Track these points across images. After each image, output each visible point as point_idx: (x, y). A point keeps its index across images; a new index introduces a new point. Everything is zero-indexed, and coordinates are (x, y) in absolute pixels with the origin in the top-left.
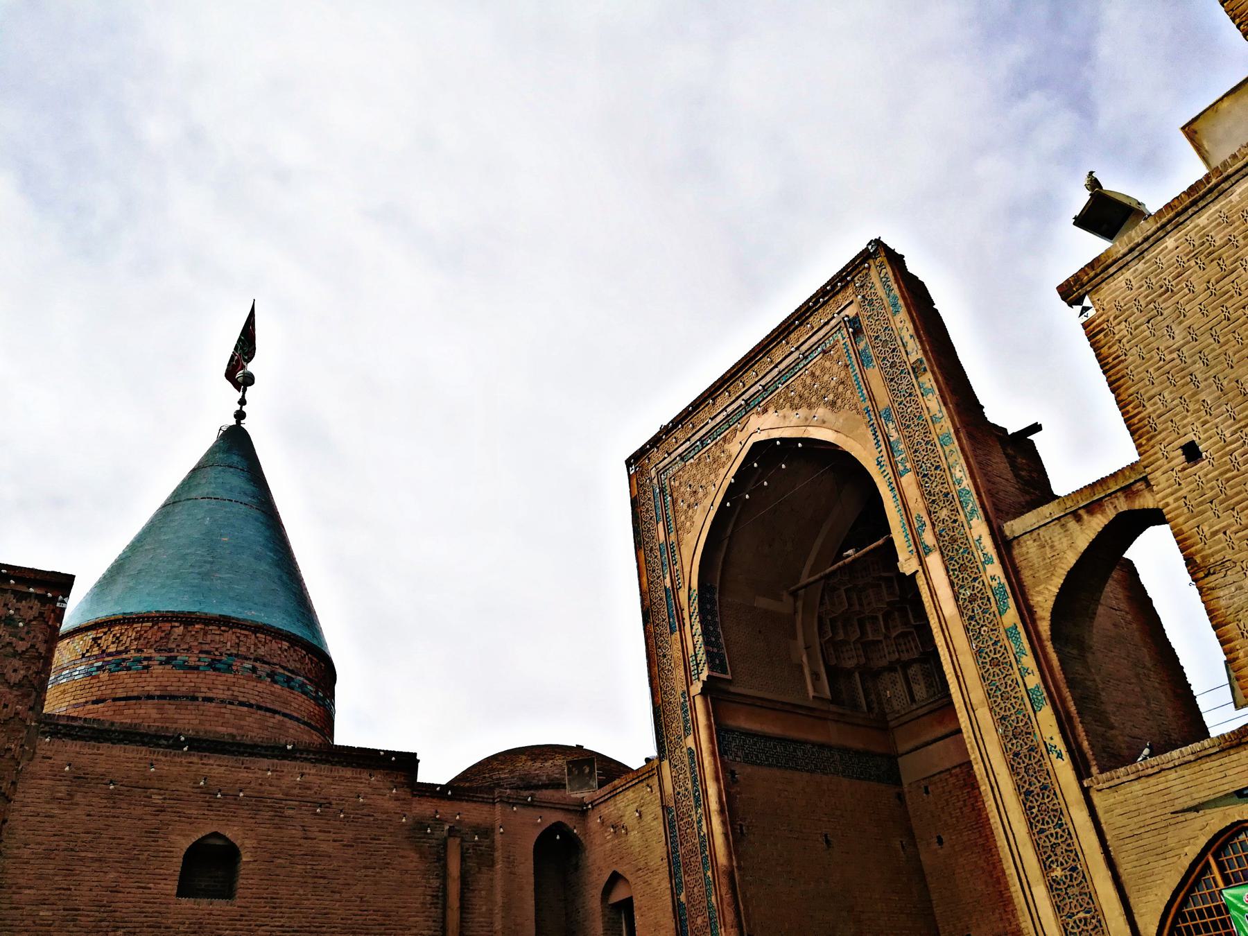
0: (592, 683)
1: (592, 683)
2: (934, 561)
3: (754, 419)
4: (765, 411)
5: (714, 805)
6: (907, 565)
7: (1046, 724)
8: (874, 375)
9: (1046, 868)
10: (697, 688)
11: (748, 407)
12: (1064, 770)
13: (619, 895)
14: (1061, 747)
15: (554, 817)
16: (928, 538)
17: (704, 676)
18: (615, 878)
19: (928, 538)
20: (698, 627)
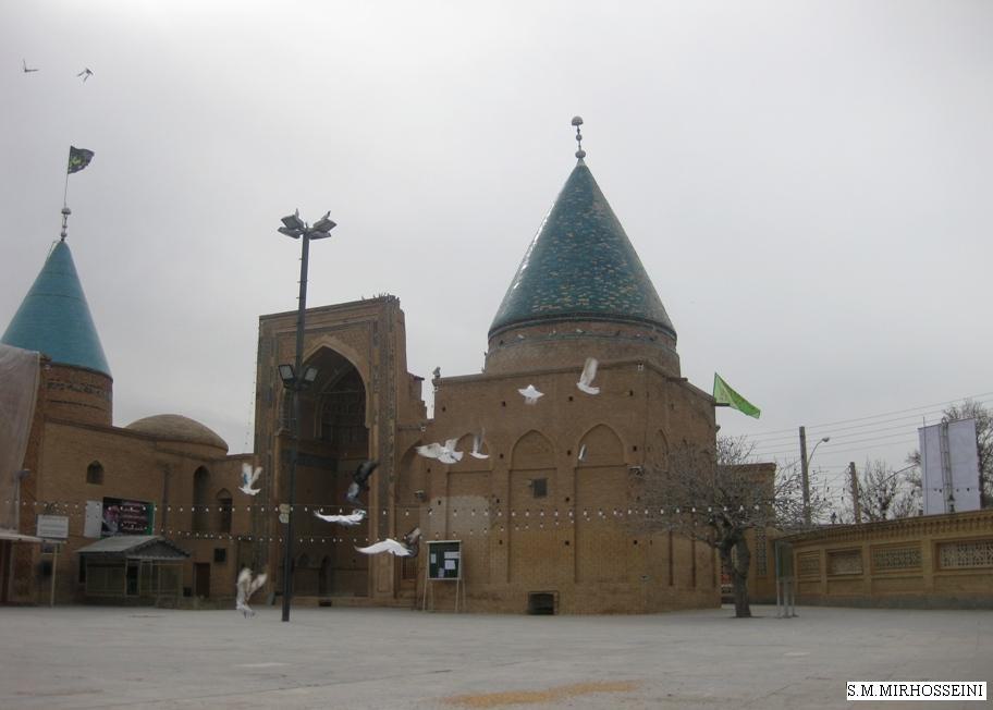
0: (226, 405)
1: (226, 405)
2: (376, 427)
3: (326, 336)
4: (331, 335)
5: (276, 478)
6: (368, 424)
7: (391, 486)
8: (376, 350)
9: (380, 522)
10: (277, 434)
11: (324, 330)
12: (392, 500)
13: (225, 496)
14: (393, 492)
15: (201, 464)
16: (377, 418)
17: (281, 429)
18: (224, 490)
19: (377, 418)
20: (282, 409)
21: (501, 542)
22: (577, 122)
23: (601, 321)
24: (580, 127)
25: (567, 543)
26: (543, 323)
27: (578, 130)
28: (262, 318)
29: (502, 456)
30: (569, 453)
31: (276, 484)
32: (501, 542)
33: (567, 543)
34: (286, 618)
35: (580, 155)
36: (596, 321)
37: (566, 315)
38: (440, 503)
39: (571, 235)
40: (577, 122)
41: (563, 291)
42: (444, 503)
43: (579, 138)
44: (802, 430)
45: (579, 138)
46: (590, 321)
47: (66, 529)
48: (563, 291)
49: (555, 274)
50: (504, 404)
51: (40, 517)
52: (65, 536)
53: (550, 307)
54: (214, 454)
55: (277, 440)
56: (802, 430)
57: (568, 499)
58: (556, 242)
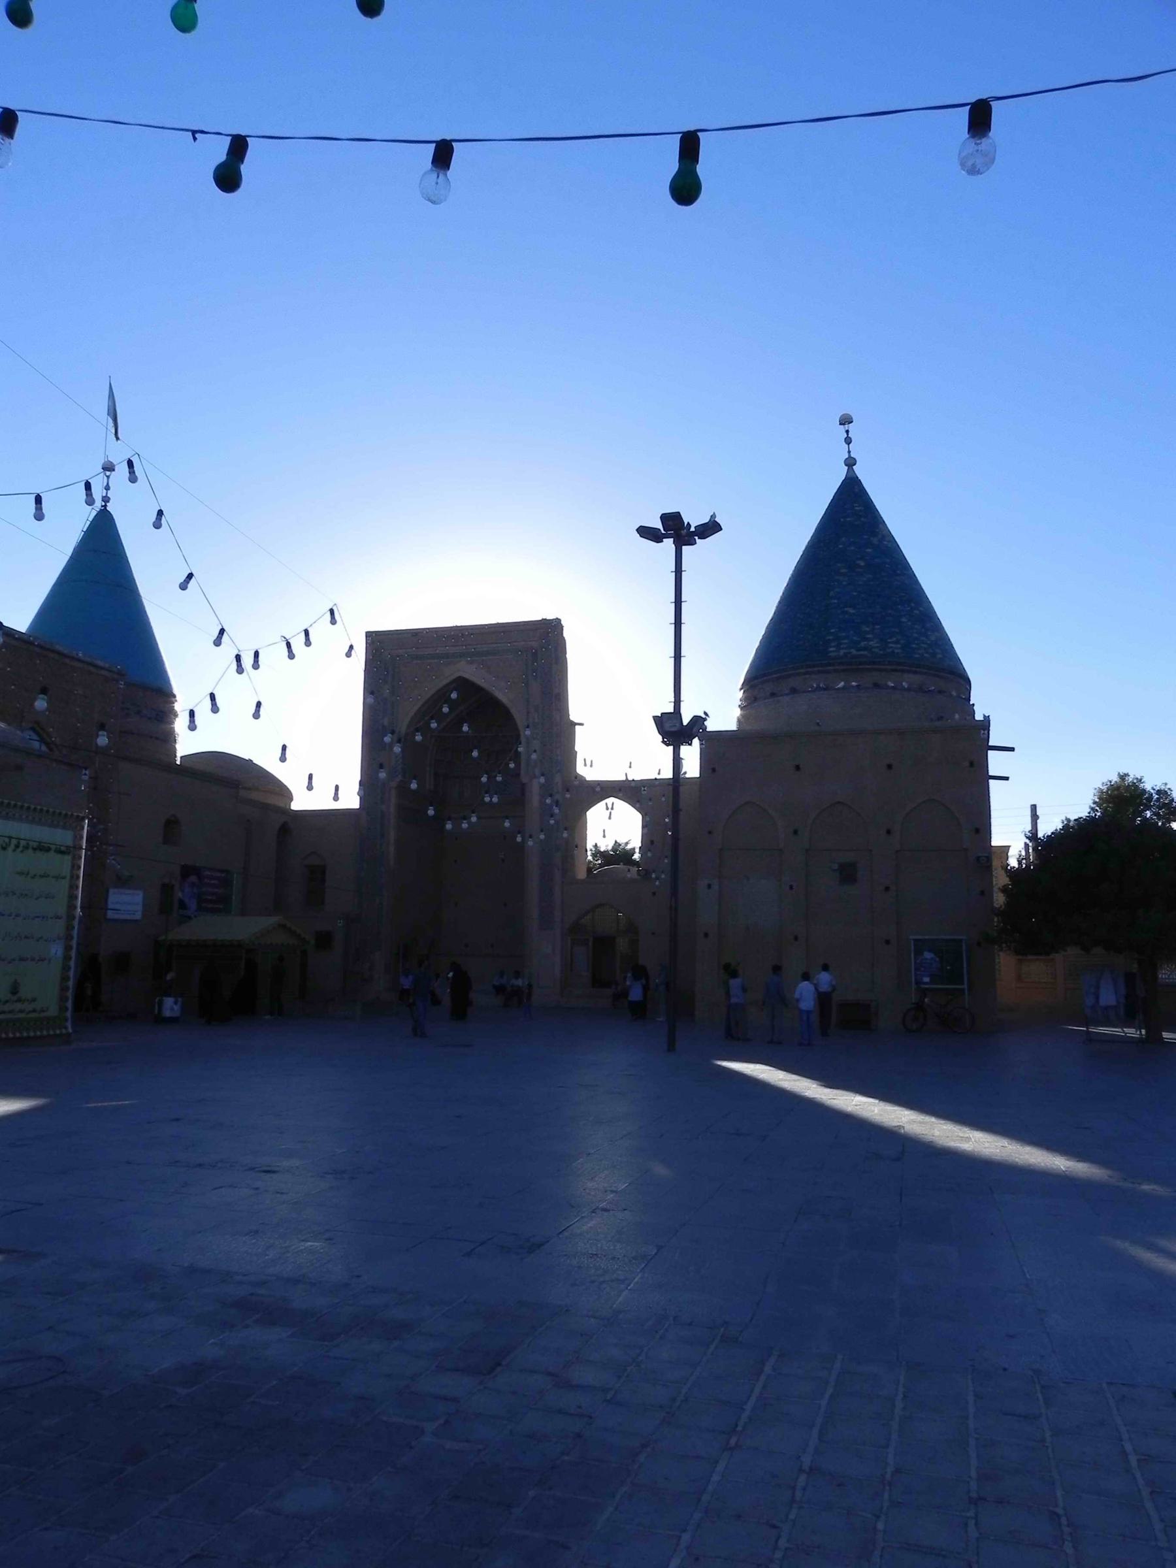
4: (471, 663)
10: (394, 784)
11: (462, 655)
21: (796, 938)
22: (846, 420)
23: (915, 673)
24: (851, 427)
25: (888, 942)
26: (844, 670)
27: (847, 432)
28: (369, 635)
29: (796, 832)
30: (889, 832)
31: (392, 849)
32: (796, 938)
33: (888, 942)
34: (671, 1047)
35: (850, 463)
36: (909, 672)
37: (874, 663)
38: (709, 886)
39: (862, 564)
40: (846, 420)
41: (868, 633)
42: (716, 887)
43: (848, 441)
44: (1034, 808)
45: (848, 441)
46: (903, 671)
47: (140, 908)
48: (868, 633)
49: (851, 611)
50: (798, 768)
51: (111, 891)
52: (138, 916)
53: (854, 651)
54: (272, 800)
55: (393, 792)
56: (1034, 808)
57: (887, 889)
58: (843, 571)
